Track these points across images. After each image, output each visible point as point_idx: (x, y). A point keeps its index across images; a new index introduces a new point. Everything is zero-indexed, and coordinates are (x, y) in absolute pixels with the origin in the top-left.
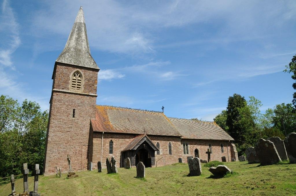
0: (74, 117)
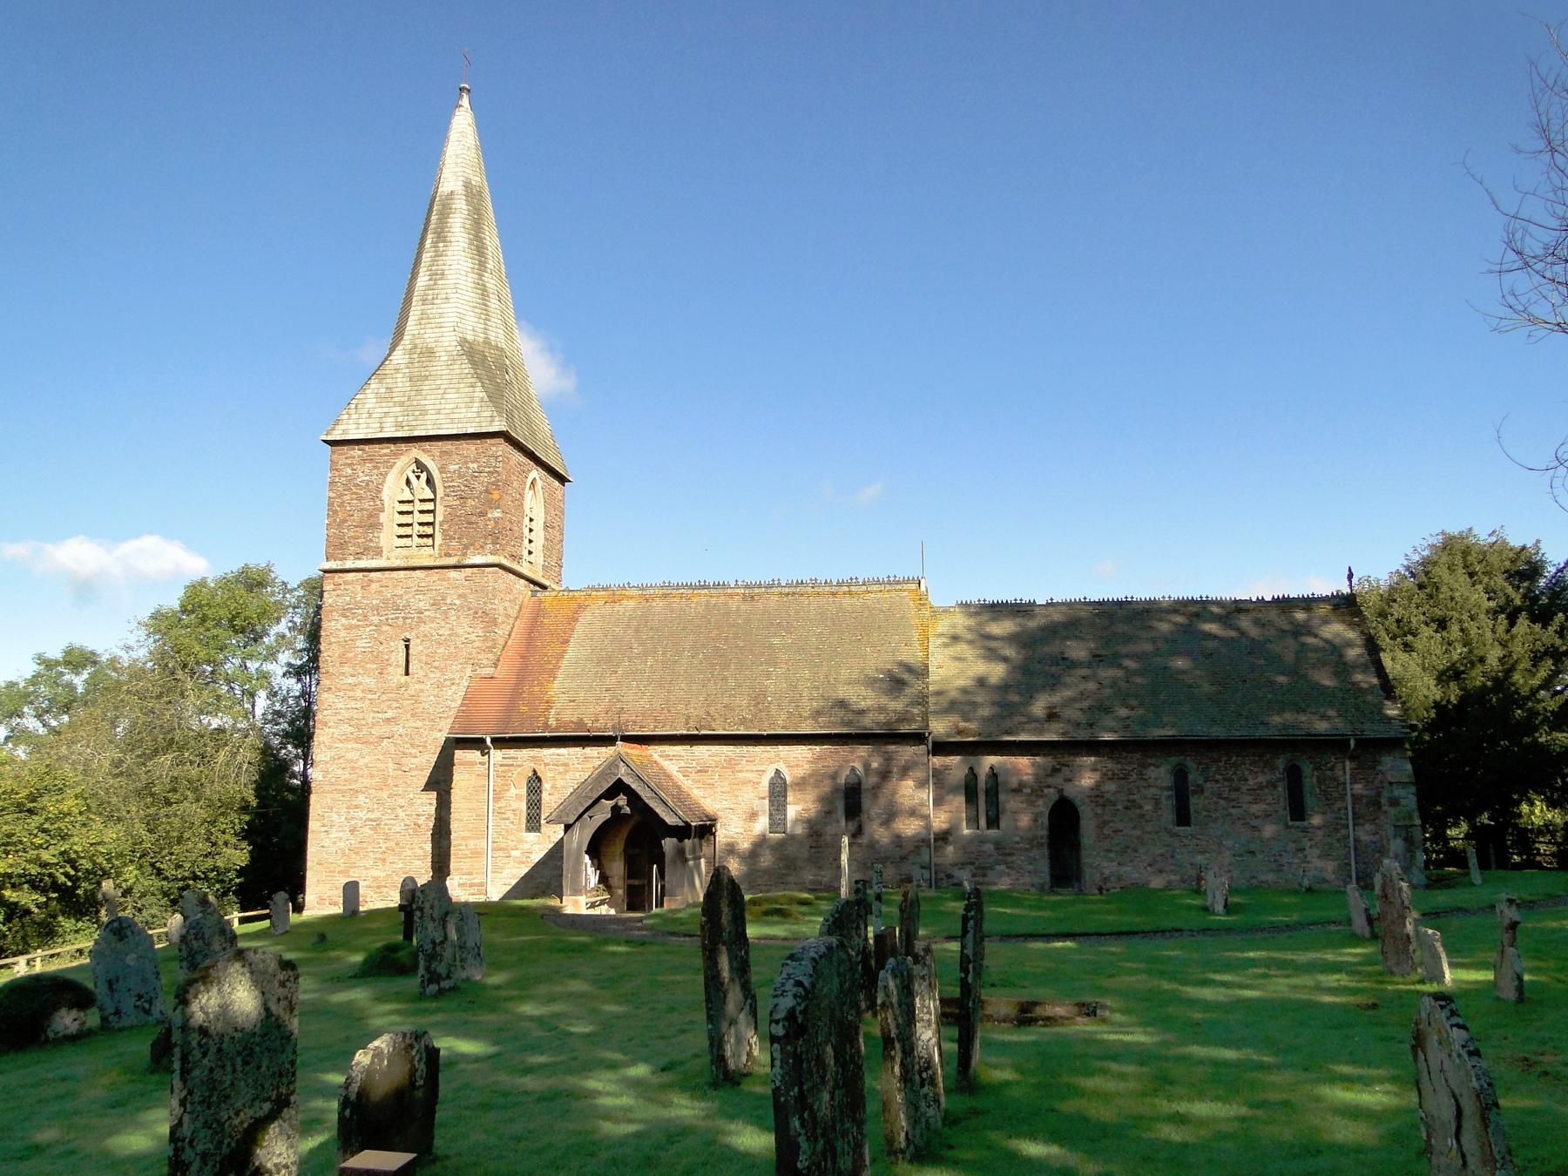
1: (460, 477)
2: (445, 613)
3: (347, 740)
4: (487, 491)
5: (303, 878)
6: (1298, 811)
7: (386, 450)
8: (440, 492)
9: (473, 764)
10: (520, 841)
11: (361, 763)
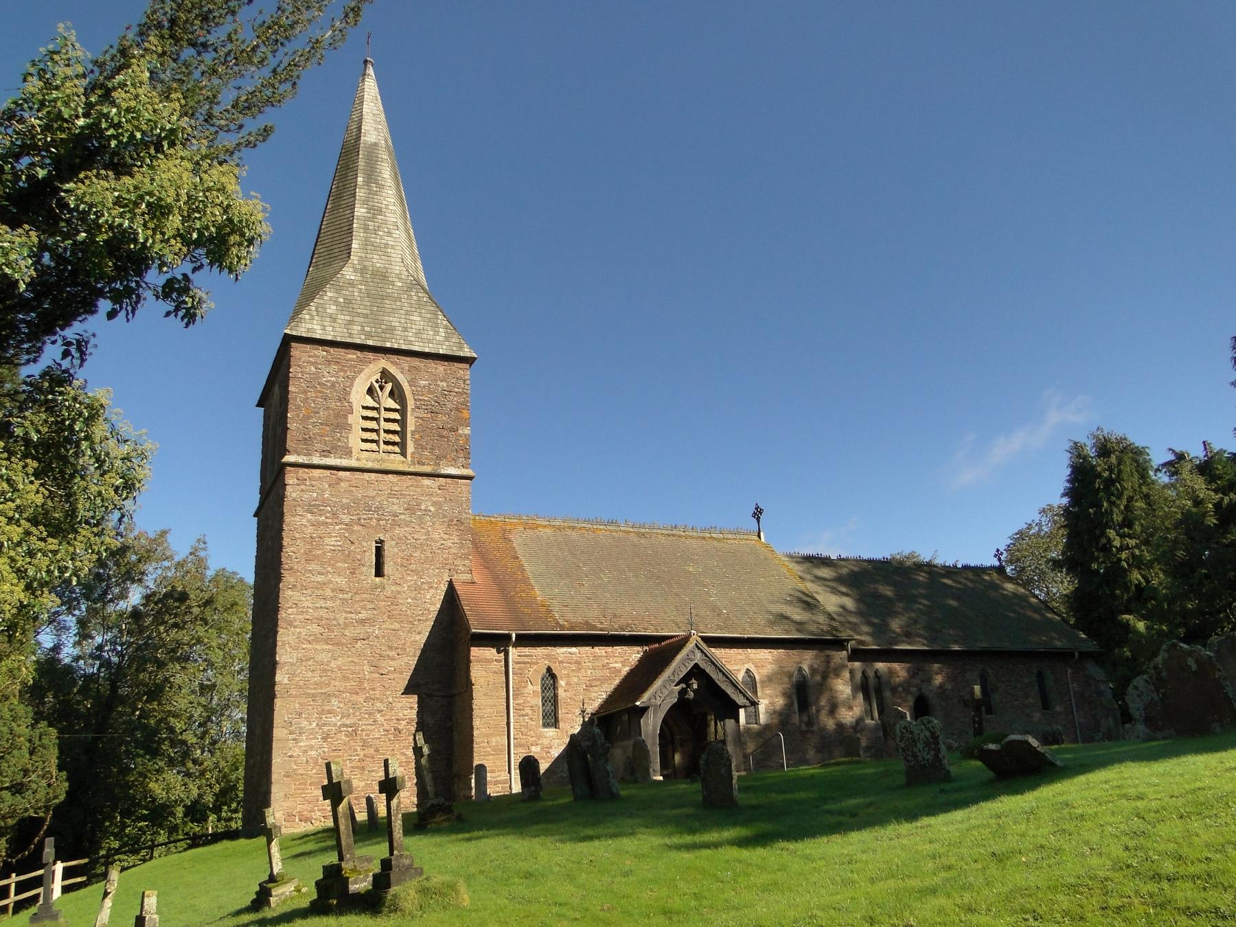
0: (379, 572)
1: (430, 392)
2: (420, 518)
3: (317, 640)
4: (457, 409)
5: (268, 793)
6: (1046, 704)
7: (353, 355)
8: (411, 404)
9: (490, 661)
10: (540, 736)
11: (333, 665)
